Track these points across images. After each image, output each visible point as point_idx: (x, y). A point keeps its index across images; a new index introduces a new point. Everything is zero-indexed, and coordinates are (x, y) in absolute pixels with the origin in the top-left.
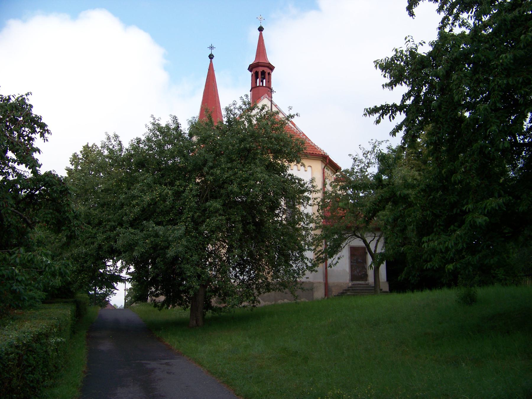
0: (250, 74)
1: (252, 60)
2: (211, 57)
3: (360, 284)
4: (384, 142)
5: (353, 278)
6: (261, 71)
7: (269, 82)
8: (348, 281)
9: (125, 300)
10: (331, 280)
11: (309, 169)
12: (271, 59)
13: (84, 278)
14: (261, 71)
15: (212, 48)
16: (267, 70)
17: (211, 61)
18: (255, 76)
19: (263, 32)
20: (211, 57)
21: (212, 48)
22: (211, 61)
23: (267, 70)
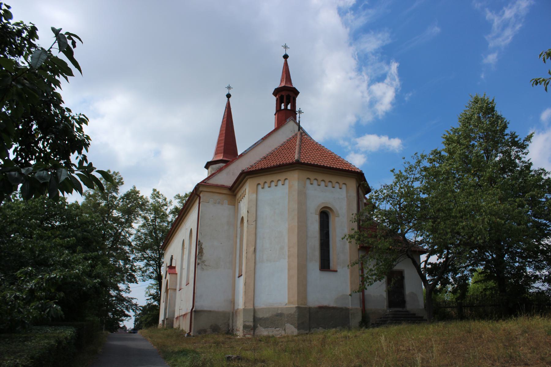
0: (274, 99)
1: (277, 83)
2: (229, 96)
3: (400, 311)
4: (181, 318)
5: (391, 304)
6: (286, 95)
7: (294, 106)
8: (385, 308)
9: (135, 324)
10: (370, 306)
11: (344, 186)
12: (295, 84)
13: (98, 225)
14: (286, 95)
15: (229, 88)
16: (291, 94)
17: (228, 100)
18: (279, 102)
19: (288, 60)
20: (229, 96)
21: (229, 88)
22: (228, 100)
23: (291, 94)
